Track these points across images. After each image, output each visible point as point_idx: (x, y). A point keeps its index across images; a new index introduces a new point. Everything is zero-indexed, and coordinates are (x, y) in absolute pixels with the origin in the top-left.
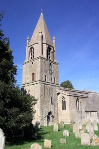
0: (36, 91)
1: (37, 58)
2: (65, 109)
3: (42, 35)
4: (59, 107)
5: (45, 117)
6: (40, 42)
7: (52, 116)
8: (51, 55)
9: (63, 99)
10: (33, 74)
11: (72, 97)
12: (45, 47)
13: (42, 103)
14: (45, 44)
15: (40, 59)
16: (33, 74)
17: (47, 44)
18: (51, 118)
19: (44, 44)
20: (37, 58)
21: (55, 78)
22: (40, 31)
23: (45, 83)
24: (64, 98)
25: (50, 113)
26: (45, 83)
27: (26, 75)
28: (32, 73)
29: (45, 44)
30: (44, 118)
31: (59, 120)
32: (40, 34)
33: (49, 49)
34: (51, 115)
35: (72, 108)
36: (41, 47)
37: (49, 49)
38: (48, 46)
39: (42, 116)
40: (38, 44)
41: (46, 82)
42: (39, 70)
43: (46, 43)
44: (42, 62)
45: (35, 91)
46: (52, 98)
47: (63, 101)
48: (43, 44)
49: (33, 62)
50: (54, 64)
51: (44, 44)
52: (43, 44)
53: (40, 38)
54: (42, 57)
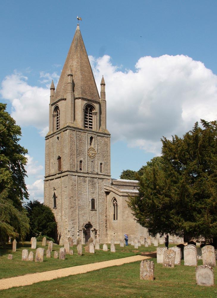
0: (64, 189)
1: (65, 129)
2: (117, 219)
3: (73, 81)
4: (109, 215)
5: (78, 232)
6: (69, 97)
7: (93, 231)
8: (93, 121)
9: (114, 201)
10: (59, 158)
11: (114, 193)
12: (80, 104)
13: (72, 209)
14: (79, 98)
15: (68, 130)
16: (59, 158)
17: (83, 99)
18: (92, 234)
19: (77, 98)
20: (65, 129)
21: (101, 164)
22: (69, 73)
23: (80, 174)
24: (115, 199)
25: (89, 226)
26: (80, 174)
27: (50, 160)
28: (57, 157)
29: (80, 100)
30: (78, 233)
31: (108, 236)
32: (69, 79)
33: (89, 109)
34: (92, 229)
35: (128, 217)
36: (70, 105)
37: (89, 109)
38: (86, 102)
39: (73, 230)
40: (65, 99)
41: (80, 173)
42: (67, 151)
43: (80, 96)
44: (72, 136)
45: (62, 188)
46: (93, 201)
47: (114, 205)
48: (75, 100)
49: (93, 136)
50: (99, 138)
51: (77, 98)
52: (75, 99)
53: (70, 88)
54: (72, 127)
